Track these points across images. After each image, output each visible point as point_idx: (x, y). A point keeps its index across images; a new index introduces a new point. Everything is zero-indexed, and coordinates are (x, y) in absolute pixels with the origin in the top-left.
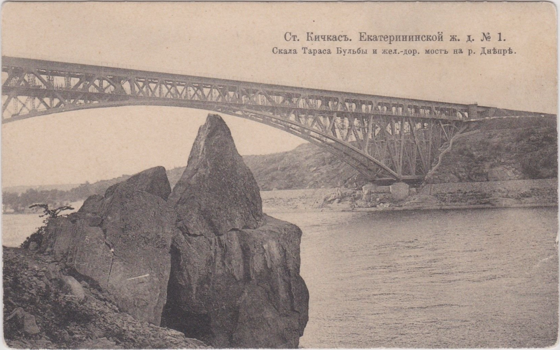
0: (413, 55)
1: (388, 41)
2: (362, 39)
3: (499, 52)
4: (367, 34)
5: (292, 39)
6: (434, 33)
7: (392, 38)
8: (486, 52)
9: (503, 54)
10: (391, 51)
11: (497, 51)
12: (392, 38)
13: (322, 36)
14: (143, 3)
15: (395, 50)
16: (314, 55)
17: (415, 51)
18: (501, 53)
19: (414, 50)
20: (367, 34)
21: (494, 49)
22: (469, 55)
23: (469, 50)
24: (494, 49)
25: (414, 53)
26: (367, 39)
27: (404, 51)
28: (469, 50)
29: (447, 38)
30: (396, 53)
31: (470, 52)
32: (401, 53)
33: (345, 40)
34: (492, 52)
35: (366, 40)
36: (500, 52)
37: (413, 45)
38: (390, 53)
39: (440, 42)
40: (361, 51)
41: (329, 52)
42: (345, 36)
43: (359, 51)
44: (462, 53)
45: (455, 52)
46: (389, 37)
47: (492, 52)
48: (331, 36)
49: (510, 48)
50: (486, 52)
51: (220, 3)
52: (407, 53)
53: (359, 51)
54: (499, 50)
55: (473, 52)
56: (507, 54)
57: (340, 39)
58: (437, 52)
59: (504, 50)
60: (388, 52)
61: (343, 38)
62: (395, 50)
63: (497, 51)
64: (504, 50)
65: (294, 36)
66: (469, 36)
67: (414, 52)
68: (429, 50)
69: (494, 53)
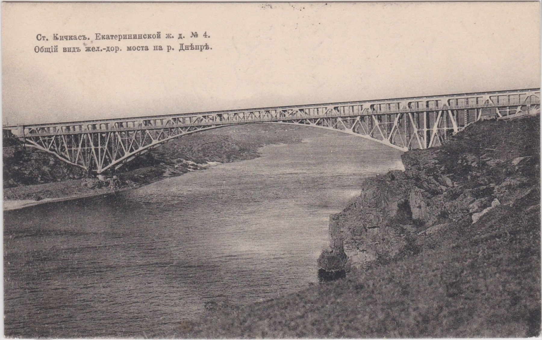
0: (116, 52)
1: (118, 40)
2: (98, 38)
3: (197, 48)
4: (101, 35)
5: (42, 39)
6: (154, 32)
7: (120, 37)
8: (184, 48)
9: (200, 50)
10: (94, 49)
11: (195, 47)
12: (120, 37)
13: (65, 37)
14: (388, 5)
15: (98, 48)
16: (201, 51)
17: (117, 48)
18: (198, 49)
19: (116, 47)
20: (101, 35)
21: (192, 45)
22: (168, 51)
23: (168, 47)
24: (192, 45)
25: (116, 50)
26: (101, 38)
27: (107, 48)
28: (168, 47)
29: (163, 35)
30: (99, 51)
31: (169, 48)
32: (103, 50)
33: (84, 39)
34: (190, 48)
35: (100, 39)
36: (117, 48)
37: (113, 43)
38: (94, 50)
39: (159, 39)
40: (44, 49)
41: (147, 49)
42: (84, 36)
43: (42, 49)
44: (162, 50)
45: (155, 48)
46: (118, 36)
47: (190, 48)
48: (104, 36)
49: (206, 44)
50: (184, 48)
51: (433, 5)
52: (110, 50)
53: (42, 49)
54: (196, 46)
55: (119, 50)
56: (204, 50)
57: (80, 38)
58: (139, 49)
59: (201, 46)
60: (91, 49)
61: (83, 38)
62: (98, 48)
63: (195, 47)
64: (201, 46)
65: (44, 37)
66: (180, 35)
67: (117, 49)
68: (131, 47)
69: (191, 49)
